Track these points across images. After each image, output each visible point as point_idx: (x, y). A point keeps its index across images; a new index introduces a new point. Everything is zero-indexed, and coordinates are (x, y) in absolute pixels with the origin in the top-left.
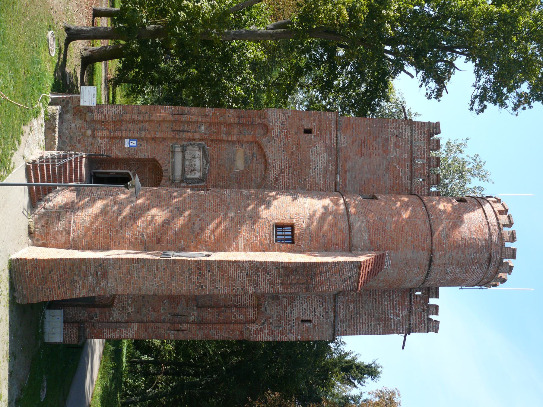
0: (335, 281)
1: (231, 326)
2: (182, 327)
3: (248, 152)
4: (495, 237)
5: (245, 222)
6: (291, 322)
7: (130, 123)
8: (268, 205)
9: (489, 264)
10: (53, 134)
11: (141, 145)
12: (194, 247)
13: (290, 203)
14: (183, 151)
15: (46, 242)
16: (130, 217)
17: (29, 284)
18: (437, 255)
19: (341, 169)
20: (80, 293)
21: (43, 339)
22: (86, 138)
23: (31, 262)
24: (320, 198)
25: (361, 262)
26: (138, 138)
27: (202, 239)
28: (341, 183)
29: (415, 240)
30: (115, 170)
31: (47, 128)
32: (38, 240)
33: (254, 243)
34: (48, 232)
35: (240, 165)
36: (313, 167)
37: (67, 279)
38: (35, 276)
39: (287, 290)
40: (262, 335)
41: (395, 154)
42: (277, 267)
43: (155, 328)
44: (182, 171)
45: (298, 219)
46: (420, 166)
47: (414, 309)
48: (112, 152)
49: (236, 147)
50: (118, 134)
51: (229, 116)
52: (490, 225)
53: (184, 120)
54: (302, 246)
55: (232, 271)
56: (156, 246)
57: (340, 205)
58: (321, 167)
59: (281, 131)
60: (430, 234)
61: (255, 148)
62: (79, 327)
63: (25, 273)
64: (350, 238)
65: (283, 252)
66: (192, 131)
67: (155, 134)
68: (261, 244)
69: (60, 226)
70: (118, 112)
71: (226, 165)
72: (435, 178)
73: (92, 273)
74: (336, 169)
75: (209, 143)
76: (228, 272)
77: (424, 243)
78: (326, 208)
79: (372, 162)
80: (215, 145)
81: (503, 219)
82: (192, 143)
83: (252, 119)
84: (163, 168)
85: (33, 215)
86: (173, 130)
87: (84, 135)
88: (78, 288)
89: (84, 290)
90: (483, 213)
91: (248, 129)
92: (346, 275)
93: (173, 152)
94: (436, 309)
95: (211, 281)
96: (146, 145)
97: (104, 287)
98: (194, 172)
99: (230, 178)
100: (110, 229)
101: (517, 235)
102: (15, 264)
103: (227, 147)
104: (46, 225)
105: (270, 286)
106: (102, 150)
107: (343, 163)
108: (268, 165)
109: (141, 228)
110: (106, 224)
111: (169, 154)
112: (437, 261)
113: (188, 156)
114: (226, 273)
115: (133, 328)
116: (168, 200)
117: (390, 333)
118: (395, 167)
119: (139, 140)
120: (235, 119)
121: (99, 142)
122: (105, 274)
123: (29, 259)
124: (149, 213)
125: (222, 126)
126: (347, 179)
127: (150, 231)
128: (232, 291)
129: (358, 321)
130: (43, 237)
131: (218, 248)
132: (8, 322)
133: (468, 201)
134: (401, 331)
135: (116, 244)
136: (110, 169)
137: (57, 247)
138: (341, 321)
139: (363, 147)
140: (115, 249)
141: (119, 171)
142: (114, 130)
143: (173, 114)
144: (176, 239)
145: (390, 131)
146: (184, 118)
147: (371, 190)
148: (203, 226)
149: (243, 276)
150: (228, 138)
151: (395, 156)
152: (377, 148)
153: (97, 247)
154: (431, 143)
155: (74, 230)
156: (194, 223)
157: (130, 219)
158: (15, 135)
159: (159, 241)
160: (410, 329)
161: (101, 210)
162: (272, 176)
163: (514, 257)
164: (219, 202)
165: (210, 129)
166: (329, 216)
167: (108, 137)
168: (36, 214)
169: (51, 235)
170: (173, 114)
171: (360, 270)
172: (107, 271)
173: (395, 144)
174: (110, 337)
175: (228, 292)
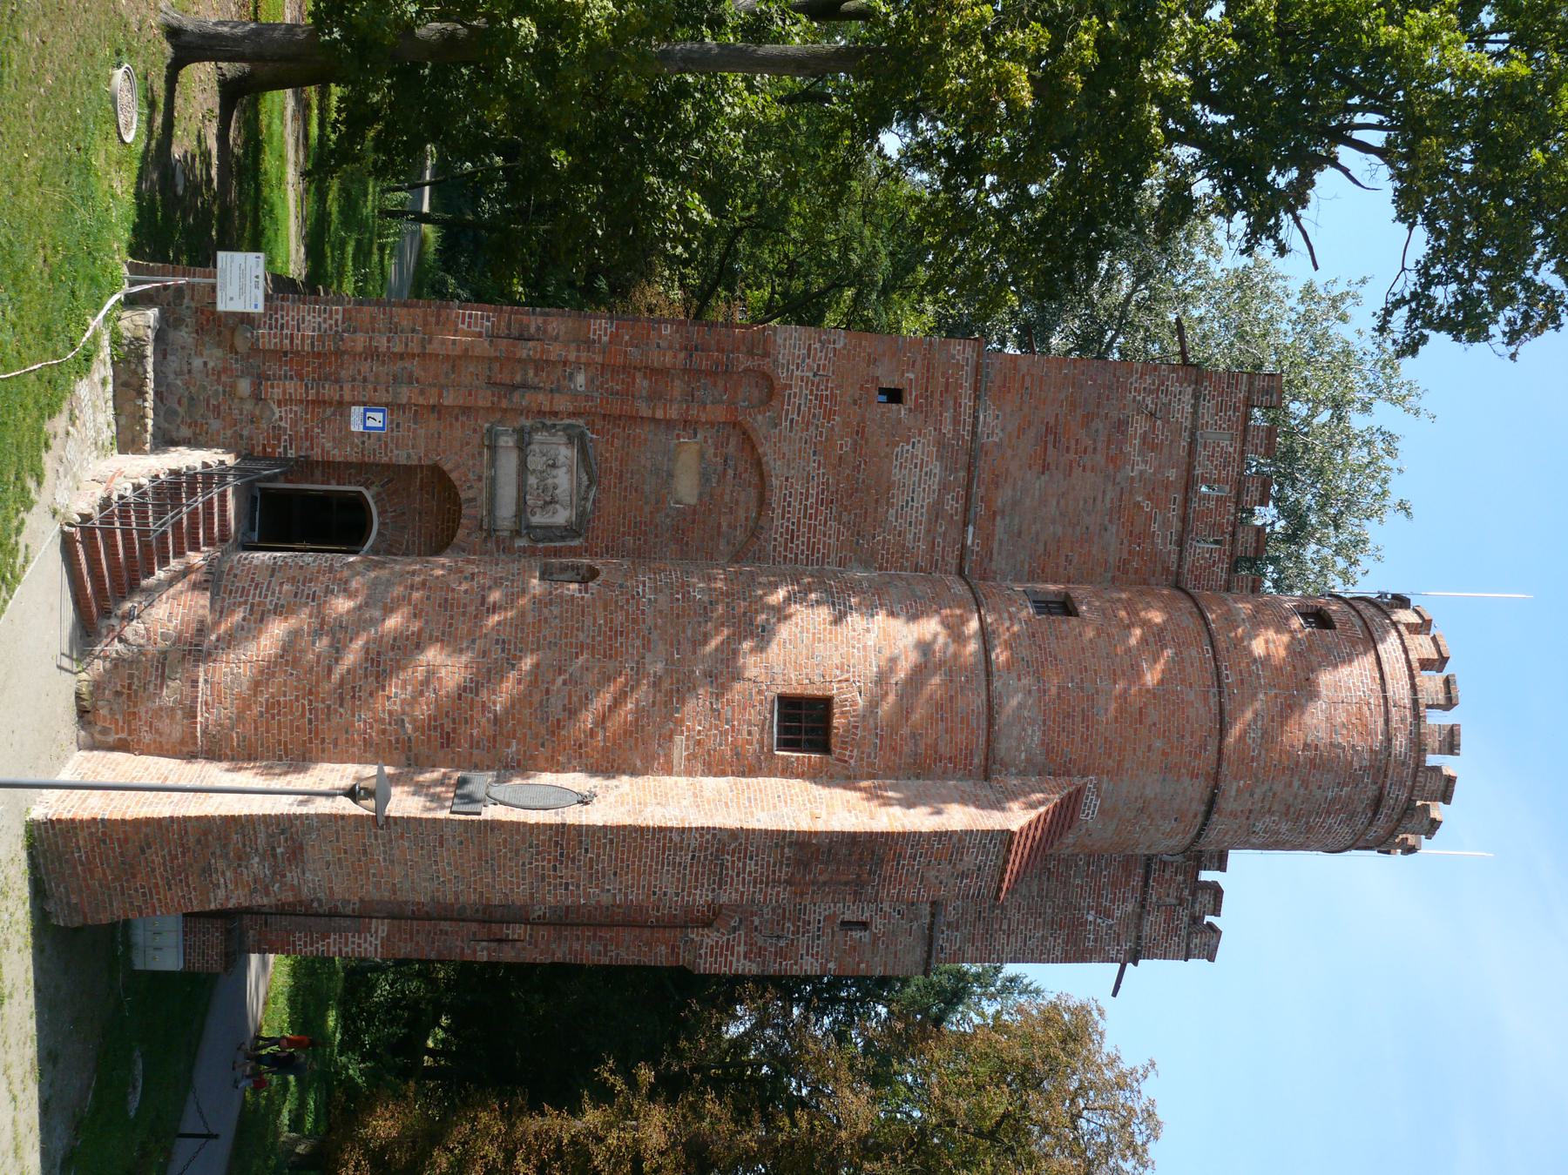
0: (937, 877)
1: (647, 933)
2: (510, 932)
3: (712, 451)
4: (1400, 743)
5: (694, 688)
6: (813, 927)
7: (366, 359)
8: (763, 636)
9: (1375, 813)
10: (140, 402)
11: (398, 425)
12: (547, 759)
13: (825, 629)
14: (522, 446)
15: (129, 738)
16: (366, 668)
17: (85, 879)
18: (1231, 788)
19: (980, 509)
20: (228, 898)
21: (129, 961)
22: (236, 401)
23: (88, 827)
24: (913, 617)
25: (1013, 833)
26: (390, 407)
27: (569, 737)
28: (976, 549)
29: (1172, 748)
30: (323, 483)
31: (119, 381)
32: (104, 731)
33: (715, 750)
34: (132, 710)
35: (686, 489)
36: (898, 501)
37: (191, 865)
38: (101, 859)
39: (801, 896)
40: (729, 958)
41: (1142, 467)
42: (777, 844)
43: (435, 934)
44: (518, 504)
45: (844, 685)
46: (1212, 505)
47: (1154, 899)
48: (312, 444)
49: (678, 436)
50: (329, 391)
51: (658, 346)
52: (1391, 703)
53: (524, 356)
54: (852, 761)
55: (652, 851)
56: (441, 754)
57: (969, 637)
58: (923, 501)
59: (811, 394)
60: (1216, 733)
61: (733, 441)
62: (229, 932)
63: (73, 853)
64: (988, 741)
65: (797, 777)
66: (548, 386)
67: (440, 396)
68: (737, 754)
69: (170, 694)
70: (331, 326)
71: (647, 488)
72: (1251, 538)
73: (261, 851)
74: (966, 510)
75: (599, 425)
76: (641, 853)
77: (1197, 756)
78: (925, 647)
79: (1074, 489)
80: (617, 430)
81: (1431, 683)
82: (549, 423)
83: (728, 358)
84: (463, 496)
85: (88, 660)
86: (491, 383)
87: (231, 392)
88: (223, 886)
89: (240, 891)
90: (1376, 669)
91: (715, 385)
92: (969, 861)
93: (493, 448)
94: (1215, 900)
95: (591, 875)
96: (413, 426)
97: (296, 882)
98: (551, 507)
99: (656, 526)
100: (310, 704)
101: (1465, 740)
102: (44, 835)
103: (650, 436)
104: (126, 691)
105: (755, 887)
106: (283, 438)
107: (986, 490)
108: (767, 494)
109: (398, 702)
110: (297, 688)
111: (481, 454)
112: (1228, 803)
113: (535, 462)
114: (635, 856)
115: (376, 932)
116: (476, 617)
117: (1083, 960)
118: (1138, 505)
119: (392, 410)
120: (675, 357)
121: (274, 414)
122: (296, 853)
123: (81, 821)
124: (421, 657)
125: (639, 375)
126: (997, 538)
127: (422, 711)
128: (649, 897)
129: (996, 926)
130: (121, 724)
131: (616, 765)
132: (32, 983)
133: (1338, 626)
134: (1113, 953)
135: (326, 745)
136: (307, 482)
137: (161, 752)
138: (949, 925)
139: (1050, 446)
140: (323, 761)
141: (333, 487)
142: (320, 379)
143: (493, 337)
144: (495, 736)
145: (1134, 400)
146: (525, 350)
147: (1061, 569)
148: (575, 699)
149: (680, 864)
150: (654, 413)
151: (1141, 473)
152: (1090, 450)
153: (274, 753)
154: (1249, 438)
155: (206, 704)
156: (547, 691)
157: (366, 676)
158: (26, 463)
159: (448, 740)
160: (1140, 952)
161: (284, 649)
162: (778, 524)
163: (1446, 797)
164: (622, 624)
165: (602, 383)
166: (934, 674)
167: (301, 401)
168: (98, 657)
169: (143, 718)
170: (493, 337)
171: (1009, 851)
172: (301, 844)
173: (1144, 437)
174: (312, 952)
175: (637, 899)
